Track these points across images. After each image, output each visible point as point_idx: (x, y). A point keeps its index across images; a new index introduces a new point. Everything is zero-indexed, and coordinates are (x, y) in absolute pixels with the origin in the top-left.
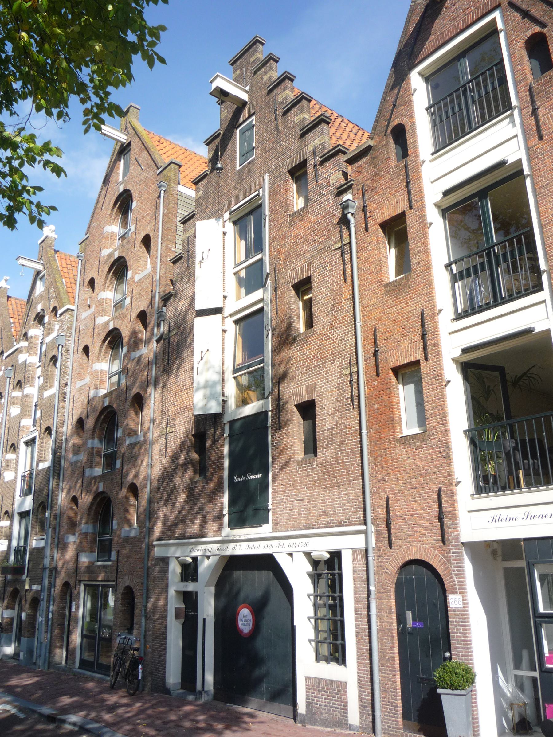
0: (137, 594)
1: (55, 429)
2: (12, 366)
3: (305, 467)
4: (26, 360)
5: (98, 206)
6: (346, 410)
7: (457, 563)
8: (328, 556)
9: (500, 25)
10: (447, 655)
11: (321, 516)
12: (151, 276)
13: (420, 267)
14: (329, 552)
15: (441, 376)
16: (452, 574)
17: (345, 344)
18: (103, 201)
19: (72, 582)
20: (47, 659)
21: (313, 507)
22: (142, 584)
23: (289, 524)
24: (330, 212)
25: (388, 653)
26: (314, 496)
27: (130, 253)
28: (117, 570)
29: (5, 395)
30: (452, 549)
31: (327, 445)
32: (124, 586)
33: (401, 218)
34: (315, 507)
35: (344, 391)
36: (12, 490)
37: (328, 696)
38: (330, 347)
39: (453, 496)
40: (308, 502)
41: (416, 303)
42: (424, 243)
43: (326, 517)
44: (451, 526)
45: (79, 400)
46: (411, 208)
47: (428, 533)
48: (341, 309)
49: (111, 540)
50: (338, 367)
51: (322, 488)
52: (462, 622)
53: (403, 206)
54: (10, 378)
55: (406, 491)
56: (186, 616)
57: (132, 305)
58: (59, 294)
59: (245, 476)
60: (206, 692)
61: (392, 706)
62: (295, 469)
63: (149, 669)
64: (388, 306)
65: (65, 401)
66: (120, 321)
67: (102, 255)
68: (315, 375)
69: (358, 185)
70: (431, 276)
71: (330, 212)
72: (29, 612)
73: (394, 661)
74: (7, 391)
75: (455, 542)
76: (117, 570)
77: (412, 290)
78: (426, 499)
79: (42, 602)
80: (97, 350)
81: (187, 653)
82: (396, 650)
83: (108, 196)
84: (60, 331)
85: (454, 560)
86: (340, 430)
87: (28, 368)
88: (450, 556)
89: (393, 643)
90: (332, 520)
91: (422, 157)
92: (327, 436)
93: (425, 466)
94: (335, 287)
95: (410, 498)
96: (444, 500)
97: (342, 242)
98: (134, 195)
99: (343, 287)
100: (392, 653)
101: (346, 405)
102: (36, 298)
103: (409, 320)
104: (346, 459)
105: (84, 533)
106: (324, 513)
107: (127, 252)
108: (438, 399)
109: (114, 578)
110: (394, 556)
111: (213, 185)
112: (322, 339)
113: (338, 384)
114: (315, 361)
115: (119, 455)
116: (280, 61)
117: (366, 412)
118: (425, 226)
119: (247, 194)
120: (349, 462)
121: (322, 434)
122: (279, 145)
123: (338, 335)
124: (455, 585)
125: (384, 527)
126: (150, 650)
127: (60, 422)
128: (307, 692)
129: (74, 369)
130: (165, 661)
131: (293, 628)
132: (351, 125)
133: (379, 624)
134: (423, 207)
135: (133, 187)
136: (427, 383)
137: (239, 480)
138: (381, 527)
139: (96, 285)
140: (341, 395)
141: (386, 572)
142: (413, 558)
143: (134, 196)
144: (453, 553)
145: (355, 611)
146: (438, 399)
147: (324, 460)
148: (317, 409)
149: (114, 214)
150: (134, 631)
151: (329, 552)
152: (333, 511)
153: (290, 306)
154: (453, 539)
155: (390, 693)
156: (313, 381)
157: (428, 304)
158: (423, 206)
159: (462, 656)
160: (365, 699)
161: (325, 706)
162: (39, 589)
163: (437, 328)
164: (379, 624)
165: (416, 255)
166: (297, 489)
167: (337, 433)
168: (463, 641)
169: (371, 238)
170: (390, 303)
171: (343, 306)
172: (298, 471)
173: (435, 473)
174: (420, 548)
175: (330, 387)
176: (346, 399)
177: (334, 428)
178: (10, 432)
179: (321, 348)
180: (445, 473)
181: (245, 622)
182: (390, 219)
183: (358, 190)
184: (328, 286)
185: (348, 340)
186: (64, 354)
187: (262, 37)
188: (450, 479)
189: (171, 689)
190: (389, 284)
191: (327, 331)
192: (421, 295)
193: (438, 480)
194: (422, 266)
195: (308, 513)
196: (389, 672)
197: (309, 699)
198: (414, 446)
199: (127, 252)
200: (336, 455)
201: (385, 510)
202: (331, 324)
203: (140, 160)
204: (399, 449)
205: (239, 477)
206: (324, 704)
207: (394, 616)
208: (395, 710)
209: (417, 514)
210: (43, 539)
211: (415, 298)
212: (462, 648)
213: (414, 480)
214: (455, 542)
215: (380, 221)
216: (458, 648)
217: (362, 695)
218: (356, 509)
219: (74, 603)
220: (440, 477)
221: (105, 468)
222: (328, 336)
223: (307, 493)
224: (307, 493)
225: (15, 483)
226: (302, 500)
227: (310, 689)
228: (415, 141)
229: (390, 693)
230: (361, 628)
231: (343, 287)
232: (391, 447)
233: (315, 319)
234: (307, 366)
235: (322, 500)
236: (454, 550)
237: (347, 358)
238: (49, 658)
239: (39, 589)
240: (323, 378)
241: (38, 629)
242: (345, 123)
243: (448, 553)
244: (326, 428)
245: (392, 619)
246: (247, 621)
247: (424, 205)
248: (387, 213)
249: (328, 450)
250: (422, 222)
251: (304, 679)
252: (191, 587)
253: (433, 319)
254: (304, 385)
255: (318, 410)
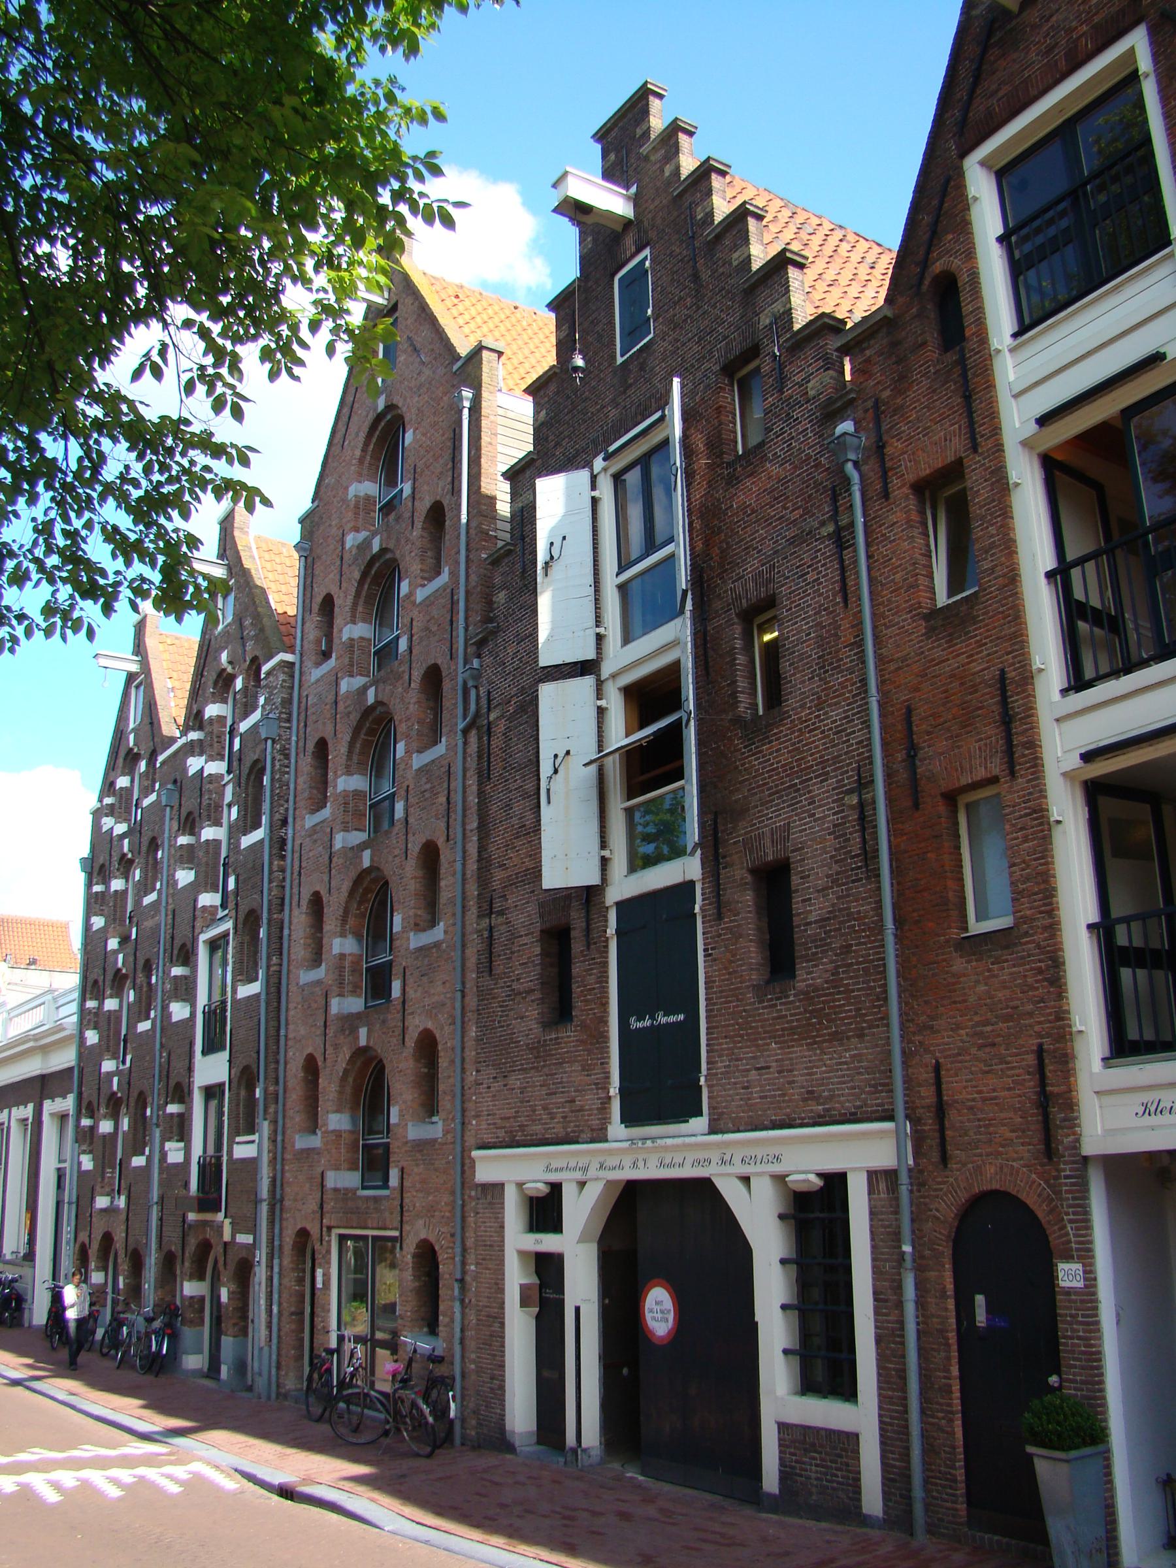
0: (442, 1257)
1: (265, 915)
2: (175, 782)
3: (771, 1000)
4: (202, 768)
5: (335, 441)
6: (853, 881)
7: (1074, 1199)
8: (818, 1182)
9: (1144, 63)
10: (1053, 1380)
11: (805, 1100)
12: (449, 590)
13: (996, 578)
14: (819, 1175)
15: (1042, 810)
16: (1063, 1219)
17: (848, 740)
18: (344, 430)
19: (314, 1230)
20: (274, 1379)
21: (790, 1083)
22: (453, 1235)
23: (741, 1118)
24: (809, 457)
25: (939, 1377)
26: (791, 1059)
27: (403, 541)
28: (402, 1206)
29: (163, 843)
30: (1064, 1170)
31: (816, 953)
32: (416, 1241)
33: (954, 471)
34: (793, 1082)
35: (848, 840)
36: (188, 1041)
37: (822, 1460)
38: (817, 747)
39: (1067, 1062)
40: (779, 1072)
41: (989, 655)
42: (1002, 526)
43: (814, 1103)
44: (1063, 1124)
45: (311, 854)
46: (975, 448)
47: (1017, 1137)
48: (839, 666)
49: (387, 1145)
50: (833, 789)
51: (807, 1044)
52: (1083, 1316)
53: (956, 447)
54: (172, 807)
55: (974, 1051)
56: (543, 1303)
57: (411, 652)
58: (262, 630)
59: (653, 1018)
60: (585, 1450)
61: (947, 1479)
62: (751, 1004)
63: (472, 1405)
64: (933, 660)
65: (283, 858)
66: (388, 688)
67: (348, 545)
68: (788, 806)
69: (865, 401)
70: (1018, 598)
71: (809, 457)
72: (233, 1287)
73: (951, 1392)
74: (166, 835)
75: (1070, 1155)
76: (402, 1206)
77: (980, 628)
78: (1013, 1068)
79: (257, 1269)
80: (344, 749)
81: (546, 1373)
82: (955, 1370)
83: (355, 418)
84: (268, 708)
85: (1067, 1192)
86: (841, 923)
87: (206, 787)
88: (1061, 1185)
89: (948, 1358)
90: (828, 1110)
91: (995, 343)
92: (815, 935)
93: (1012, 1000)
94: (825, 619)
95: (982, 1065)
96: (1049, 1068)
97: (836, 522)
98: (409, 416)
99: (842, 619)
100: (945, 1378)
101: (852, 869)
102: (216, 638)
103: (976, 691)
104: (854, 984)
105: (333, 1131)
106: (811, 1095)
107: (398, 540)
108: (1035, 859)
109: (396, 1223)
110: (952, 1185)
111: (568, 397)
112: (800, 730)
113: (835, 826)
114: (787, 776)
115: (396, 970)
116: (698, 132)
117: (892, 884)
118: (1002, 487)
119: (639, 417)
120: (858, 990)
121: (806, 930)
122: (700, 312)
123: (832, 723)
124: (1070, 1242)
125: (929, 1125)
126: (473, 1366)
127: (275, 901)
128: (780, 1452)
129: (299, 788)
130: (502, 1388)
131: (754, 1326)
132: (863, 246)
133: (920, 1319)
134: (998, 451)
135: (405, 399)
136: (1013, 825)
137: (640, 1025)
138: (925, 1124)
139: (336, 609)
140: (842, 847)
141: (935, 1216)
142: (986, 1187)
143: (407, 419)
144: (1066, 1177)
145: (875, 1293)
146: (1035, 859)
147: (810, 985)
148: (793, 878)
149: (368, 458)
150: (441, 1328)
151: (820, 1175)
152: (830, 1090)
153: (735, 659)
154: (1066, 1149)
155: (943, 1455)
156: (784, 819)
157: (1014, 657)
158: (999, 448)
159: (1082, 1382)
160: (894, 1466)
161: (817, 1479)
162: (251, 1241)
163: (1032, 708)
164: (920, 1319)
165: (987, 552)
166: (758, 1046)
167: (835, 930)
168: (1085, 1353)
169: (897, 515)
170: (938, 653)
171: (842, 659)
172: (758, 1009)
173: (1030, 1014)
174: (1001, 1168)
175: (819, 831)
176: (852, 857)
177: (829, 918)
178: (178, 920)
179: (798, 749)
180: (1050, 1014)
181: (659, 1315)
182: (932, 474)
183: (866, 411)
184: (810, 616)
185: (854, 732)
186: (278, 757)
187: (656, 81)
188: (1059, 1028)
189: (517, 1443)
190: (935, 613)
191: (810, 714)
192: (998, 638)
193: (1037, 1028)
194: (1000, 576)
195: (780, 1096)
196: (940, 1415)
197: (786, 1466)
198: (990, 957)
199: (398, 540)
200: (833, 974)
201: (933, 1089)
202: (819, 698)
203: (418, 341)
204: (959, 964)
205: (641, 1018)
206: (813, 1475)
207: (951, 1304)
208: (951, 1488)
209: (996, 1098)
210: (253, 1142)
211: (986, 644)
212: (1082, 1368)
213: (989, 1028)
214: (1070, 1155)
215: (911, 477)
216: (1075, 1367)
217: (888, 1458)
218: (875, 1086)
219: (319, 1272)
220: (1040, 1023)
221: (369, 995)
222: (814, 724)
223: (777, 1055)
224: (777, 1055)
225: (194, 1026)
226: (768, 1067)
227: (787, 1446)
228: (979, 308)
229: (943, 1455)
230: (887, 1328)
231: (842, 619)
232: (944, 960)
233: (786, 688)
234: (771, 788)
235: (806, 1068)
236: (1068, 1173)
237: (852, 770)
238: (278, 1378)
239: (251, 1241)
240: (804, 812)
241: (253, 1321)
242: (848, 242)
243: (1057, 1178)
244: (812, 918)
245: (946, 1309)
246: (662, 1312)
247: (1002, 445)
248: (927, 463)
249: (816, 966)
250: (997, 481)
251: (776, 1426)
252: (548, 1242)
253: (1024, 691)
254: (766, 826)
255: (795, 880)
